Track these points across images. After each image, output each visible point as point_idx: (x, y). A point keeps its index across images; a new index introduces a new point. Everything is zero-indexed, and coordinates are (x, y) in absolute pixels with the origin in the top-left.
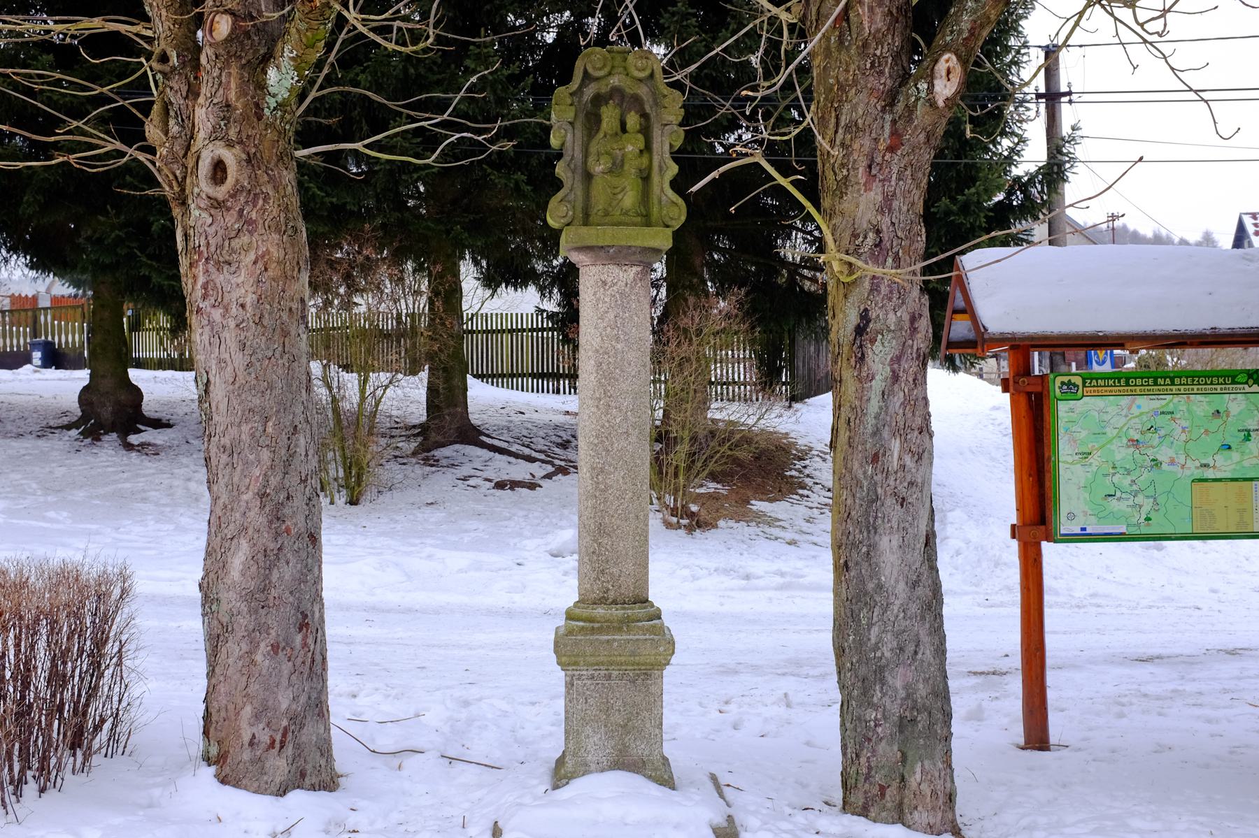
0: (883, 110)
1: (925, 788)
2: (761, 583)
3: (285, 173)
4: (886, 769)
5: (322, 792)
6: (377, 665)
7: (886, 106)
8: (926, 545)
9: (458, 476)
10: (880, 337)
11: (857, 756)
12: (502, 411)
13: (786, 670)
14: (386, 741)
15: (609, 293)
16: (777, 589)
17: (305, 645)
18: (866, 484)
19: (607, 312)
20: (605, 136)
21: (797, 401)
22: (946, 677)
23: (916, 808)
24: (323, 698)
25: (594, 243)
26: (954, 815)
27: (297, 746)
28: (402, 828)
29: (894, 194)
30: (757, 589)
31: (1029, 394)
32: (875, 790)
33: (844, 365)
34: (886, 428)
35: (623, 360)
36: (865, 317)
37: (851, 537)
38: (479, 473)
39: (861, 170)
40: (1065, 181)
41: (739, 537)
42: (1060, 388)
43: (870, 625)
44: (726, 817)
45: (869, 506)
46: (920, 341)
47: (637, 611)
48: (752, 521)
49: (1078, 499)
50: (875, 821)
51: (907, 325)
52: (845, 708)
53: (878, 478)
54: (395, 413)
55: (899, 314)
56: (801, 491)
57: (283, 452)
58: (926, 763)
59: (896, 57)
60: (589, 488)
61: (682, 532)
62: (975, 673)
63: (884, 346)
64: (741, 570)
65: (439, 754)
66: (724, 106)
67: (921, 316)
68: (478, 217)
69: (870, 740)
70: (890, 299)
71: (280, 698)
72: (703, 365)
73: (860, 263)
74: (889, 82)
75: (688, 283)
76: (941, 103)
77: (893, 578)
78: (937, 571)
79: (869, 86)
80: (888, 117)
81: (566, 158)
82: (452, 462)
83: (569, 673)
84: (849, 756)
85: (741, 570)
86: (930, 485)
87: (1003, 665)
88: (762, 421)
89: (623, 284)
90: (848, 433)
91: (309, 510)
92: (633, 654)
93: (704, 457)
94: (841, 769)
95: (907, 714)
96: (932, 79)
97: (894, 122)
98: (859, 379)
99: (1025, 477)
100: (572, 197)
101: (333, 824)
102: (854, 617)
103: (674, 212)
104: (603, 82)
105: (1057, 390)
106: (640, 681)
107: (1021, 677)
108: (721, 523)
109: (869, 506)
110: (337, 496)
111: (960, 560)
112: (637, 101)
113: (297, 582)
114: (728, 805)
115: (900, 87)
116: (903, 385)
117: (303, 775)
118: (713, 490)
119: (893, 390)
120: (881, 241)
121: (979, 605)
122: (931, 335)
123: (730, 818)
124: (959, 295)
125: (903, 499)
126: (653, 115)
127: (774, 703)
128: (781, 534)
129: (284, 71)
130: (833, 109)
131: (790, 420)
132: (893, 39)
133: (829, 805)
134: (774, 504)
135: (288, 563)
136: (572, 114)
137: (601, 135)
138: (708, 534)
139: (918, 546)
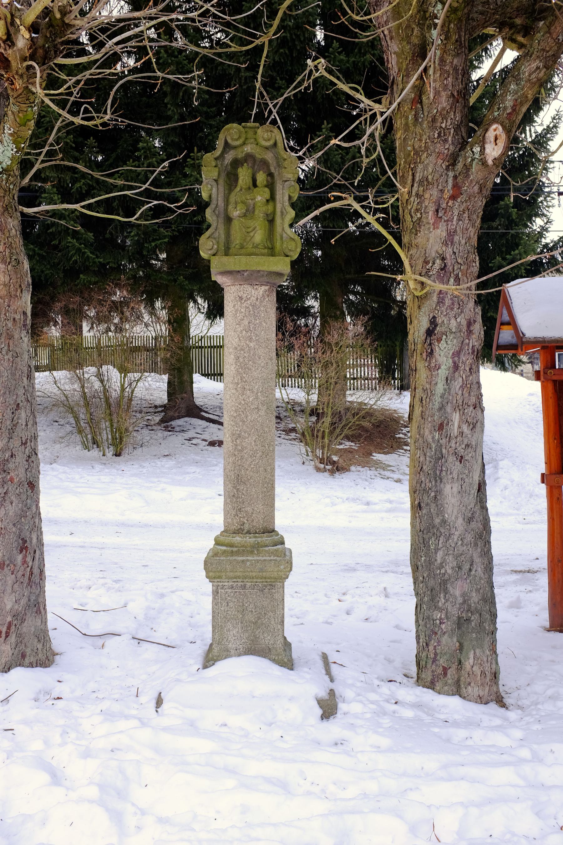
0: (447, 168)
1: (477, 670)
2: (377, 507)
3: (10, 220)
4: (448, 655)
5: (39, 669)
6: (116, 564)
7: (449, 165)
8: (479, 491)
9: (186, 438)
10: (444, 337)
11: (427, 645)
12: (218, 397)
13: (388, 569)
14: (97, 627)
15: (244, 305)
16: (386, 512)
17: (24, 562)
18: (434, 446)
19: (243, 320)
20: (241, 190)
21: (405, 390)
22: (493, 587)
23: (469, 684)
24: (40, 600)
25: (233, 268)
26: (498, 688)
27: (19, 635)
28: (95, 695)
29: (455, 231)
30: (373, 511)
31: (555, 382)
32: (440, 670)
33: (418, 358)
34: (449, 404)
35: (254, 354)
36: (433, 322)
37: (423, 485)
38: (199, 436)
39: (431, 213)
41: (364, 477)
43: (437, 550)
44: (328, 691)
45: (436, 463)
46: (474, 340)
47: (265, 539)
48: (372, 466)
50: (439, 693)
51: (464, 329)
52: (419, 609)
53: (443, 441)
54: (147, 397)
55: (458, 320)
56: (405, 447)
57: (8, 422)
58: (478, 651)
59: (457, 129)
60: (231, 449)
61: (327, 474)
62: (516, 572)
63: (447, 344)
64: (363, 499)
65: (131, 637)
66: (335, 178)
67: (475, 321)
68: (195, 270)
69: (436, 633)
70: (452, 309)
71: (6, 601)
72: (341, 366)
73: (429, 282)
74: (452, 148)
75: (333, 315)
76: (490, 162)
77: (453, 517)
78: (487, 510)
79: (437, 150)
80: (451, 174)
81: (212, 206)
82: (183, 429)
83: (214, 584)
84: (421, 644)
85: (363, 499)
86: (482, 447)
87: (535, 565)
88: (379, 402)
89: (255, 299)
90: (421, 408)
91: (29, 465)
92: (261, 570)
93: (342, 425)
94: (415, 652)
95: (464, 615)
96: (484, 143)
97: (455, 177)
98: (429, 368)
99: (551, 440)
100: (216, 235)
101: (43, 693)
102: (425, 543)
103: (292, 245)
104: (240, 150)
106: (267, 590)
107: (547, 575)
108: (353, 468)
109: (436, 463)
110: (107, 451)
111: (507, 492)
112: (264, 164)
113: (18, 517)
114: (332, 680)
115: (460, 151)
116: (462, 372)
117: (23, 656)
118: (348, 447)
119: (454, 376)
120: (445, 266)
121: (519, 523)
122: (482, 336)
123: (332, 693)
124: (505, 312)
125: (462, 457)
126: (276, 174)
127: (377, 594)
128: (392, 475)
129: (6, 144)
130: (410, 170)
131: (397, 402)
132: (454, 115)
133: (408, 677)
134: (387, 456)
135: (12, 503)
136: (216, 174)
137: (238, 189)
138: (343, 475)
139: (472, 492)
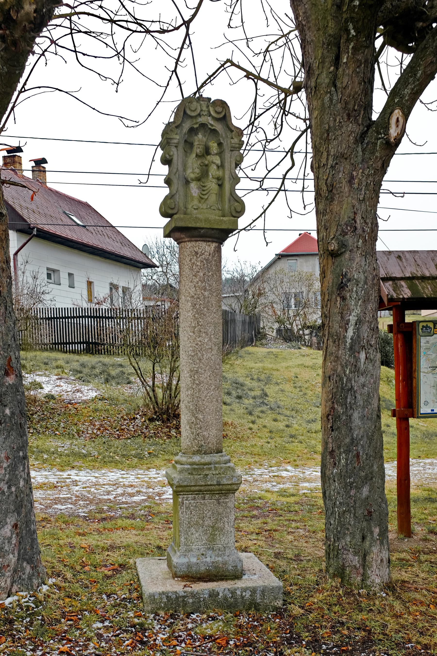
15: (199, 259)
19: (198, 272)
35: (208, 302)
40: (243, 276)
42: (422, 329)
49: (430, 393)
89: (208, 254)
105: (420, 331)
